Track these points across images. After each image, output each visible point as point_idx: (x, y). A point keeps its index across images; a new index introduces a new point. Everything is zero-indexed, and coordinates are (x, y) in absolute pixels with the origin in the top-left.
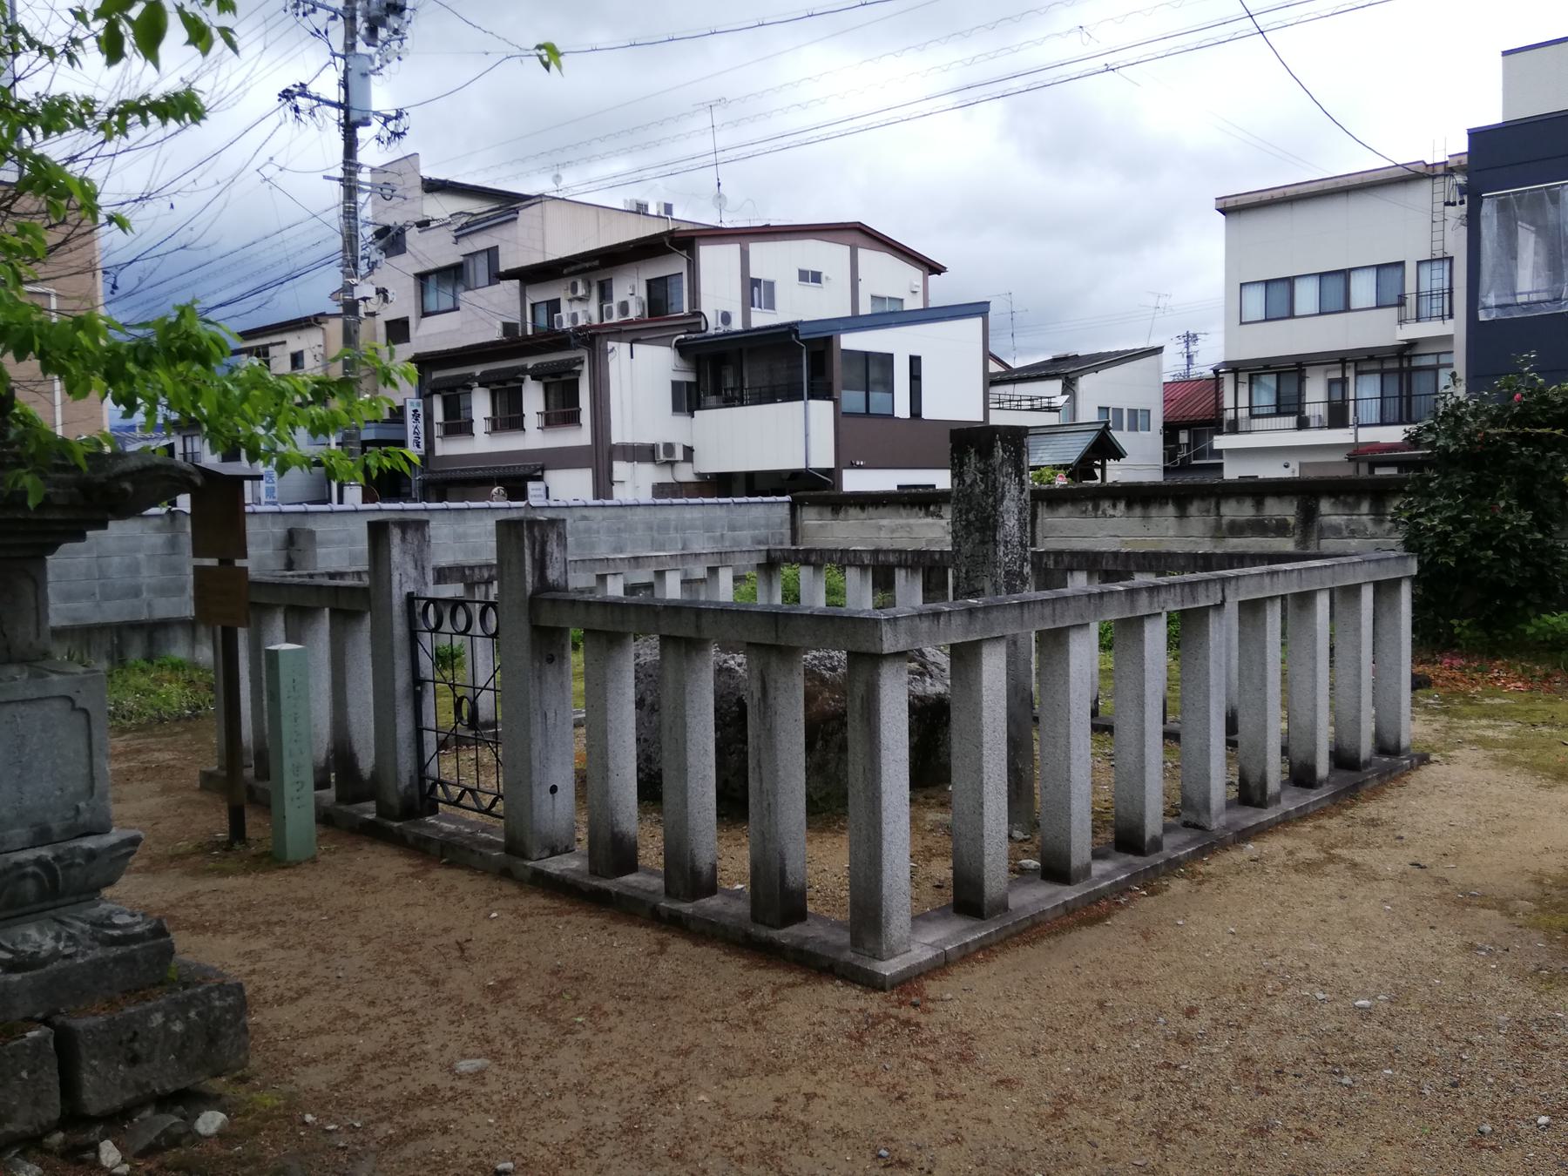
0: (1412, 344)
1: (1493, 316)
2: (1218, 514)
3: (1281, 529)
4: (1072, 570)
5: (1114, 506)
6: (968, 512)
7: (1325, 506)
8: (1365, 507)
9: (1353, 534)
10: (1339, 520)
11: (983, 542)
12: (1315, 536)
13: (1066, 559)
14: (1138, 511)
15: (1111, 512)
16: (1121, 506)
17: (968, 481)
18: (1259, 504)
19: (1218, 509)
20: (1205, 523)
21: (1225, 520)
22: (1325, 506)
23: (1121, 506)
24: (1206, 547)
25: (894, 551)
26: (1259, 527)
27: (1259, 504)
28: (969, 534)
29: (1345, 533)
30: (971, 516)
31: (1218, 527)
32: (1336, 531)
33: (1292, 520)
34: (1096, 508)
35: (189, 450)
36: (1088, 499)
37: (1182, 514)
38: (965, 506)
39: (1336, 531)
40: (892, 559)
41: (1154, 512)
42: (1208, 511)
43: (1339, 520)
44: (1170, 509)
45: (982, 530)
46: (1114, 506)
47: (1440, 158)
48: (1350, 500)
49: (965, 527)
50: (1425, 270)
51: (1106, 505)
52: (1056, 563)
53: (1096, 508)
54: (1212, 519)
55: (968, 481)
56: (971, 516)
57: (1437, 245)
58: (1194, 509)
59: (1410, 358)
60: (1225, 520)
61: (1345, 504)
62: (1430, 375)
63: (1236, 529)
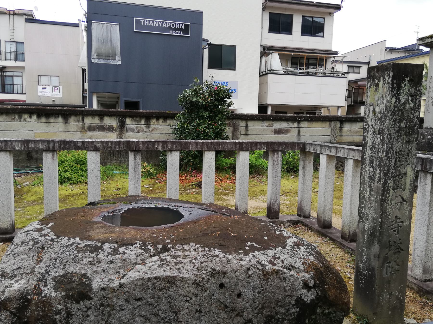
0: (4, 67)
1: (96, 62)
2: (83, 122)
3: (111, 129)
4: (171, 151)
5: (31, 117)
6: (400, 122)
7: (128, 121)
8: (143, 122)
9: (139, 131)
10: (134, 126)
11: (408, 142)
12: (125, 131)
13: (169, 146)
14: (43, 120)
15: (28, 119)
16: (34, 117)
17: (403, 100)
18: (101, 119)
19: (83, 120)
20: (77, 126)
21: (86, 125)
22: (128, 121)
23: (34, 117)
24: (77, 137)
25: (43, 141)
26: (102, 128)
27: (101, 119)
28: (399, 136)
29: (136, 131)
30: (403, 125)
31: (83, 128)
32: (132, 130)
33: (115, 126)
34: (20, 117)
35: (140, 262)
36: (16, 113)
37: (66, 122)
38: (398, 117)
39: (132, 130)
40: (41, 146)
41: (52, 120)
42: (79, 121)
43: (134, 126)
44: (60, 120)
45: (408, 134)
46: (31, 117)
47: (12, 9)
48: (137, 119)
49: (398, 131)
50: (7, 43)
51: (26, 116)
52: (163, 147)
53: (20, 117)
54: (80, 124)
55: (403, 100)
56: (403, 125)
57: (12, 37)
58: (72, 119)
59: (4, 72)
60: (86, 125)
61: (136, 120)
62: (11, 78)
63: (91, 129)
